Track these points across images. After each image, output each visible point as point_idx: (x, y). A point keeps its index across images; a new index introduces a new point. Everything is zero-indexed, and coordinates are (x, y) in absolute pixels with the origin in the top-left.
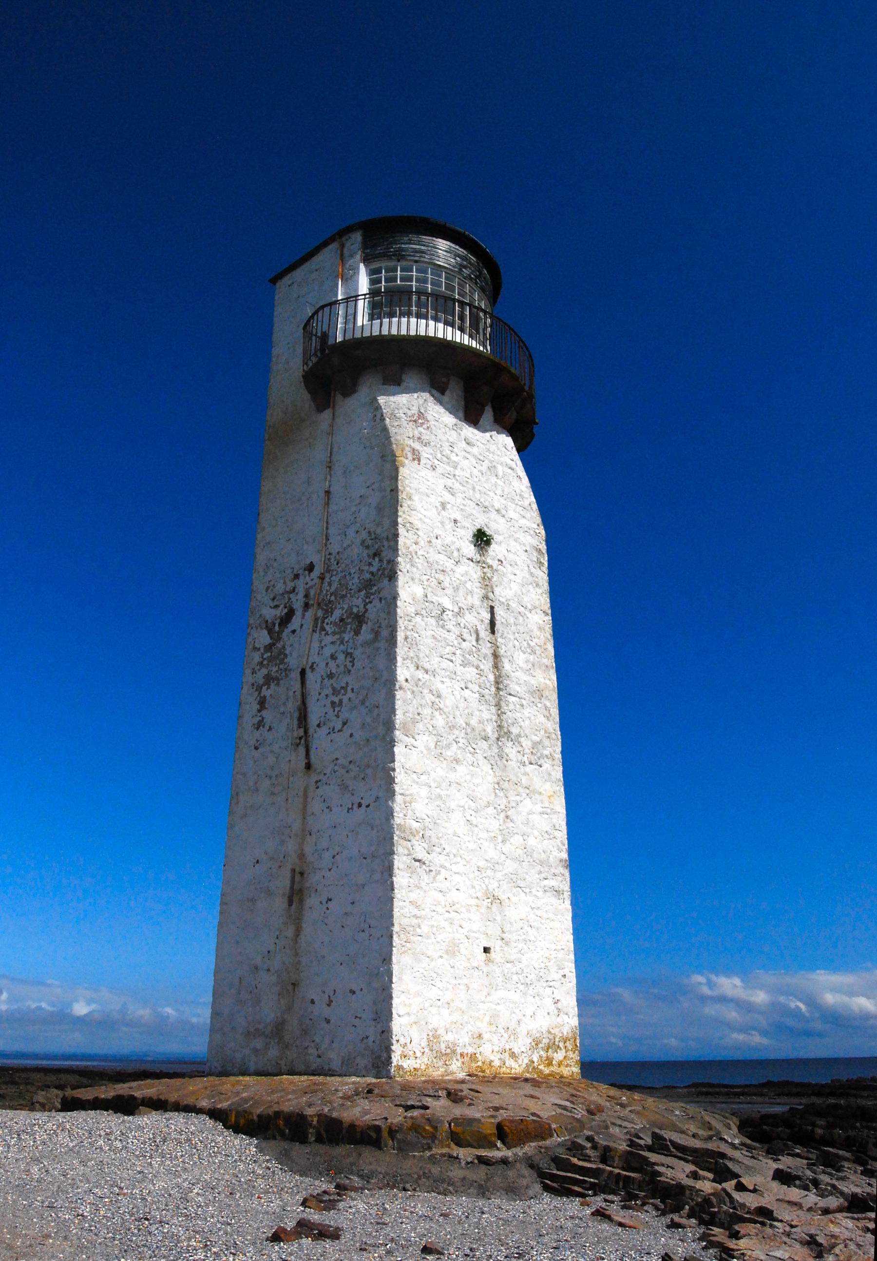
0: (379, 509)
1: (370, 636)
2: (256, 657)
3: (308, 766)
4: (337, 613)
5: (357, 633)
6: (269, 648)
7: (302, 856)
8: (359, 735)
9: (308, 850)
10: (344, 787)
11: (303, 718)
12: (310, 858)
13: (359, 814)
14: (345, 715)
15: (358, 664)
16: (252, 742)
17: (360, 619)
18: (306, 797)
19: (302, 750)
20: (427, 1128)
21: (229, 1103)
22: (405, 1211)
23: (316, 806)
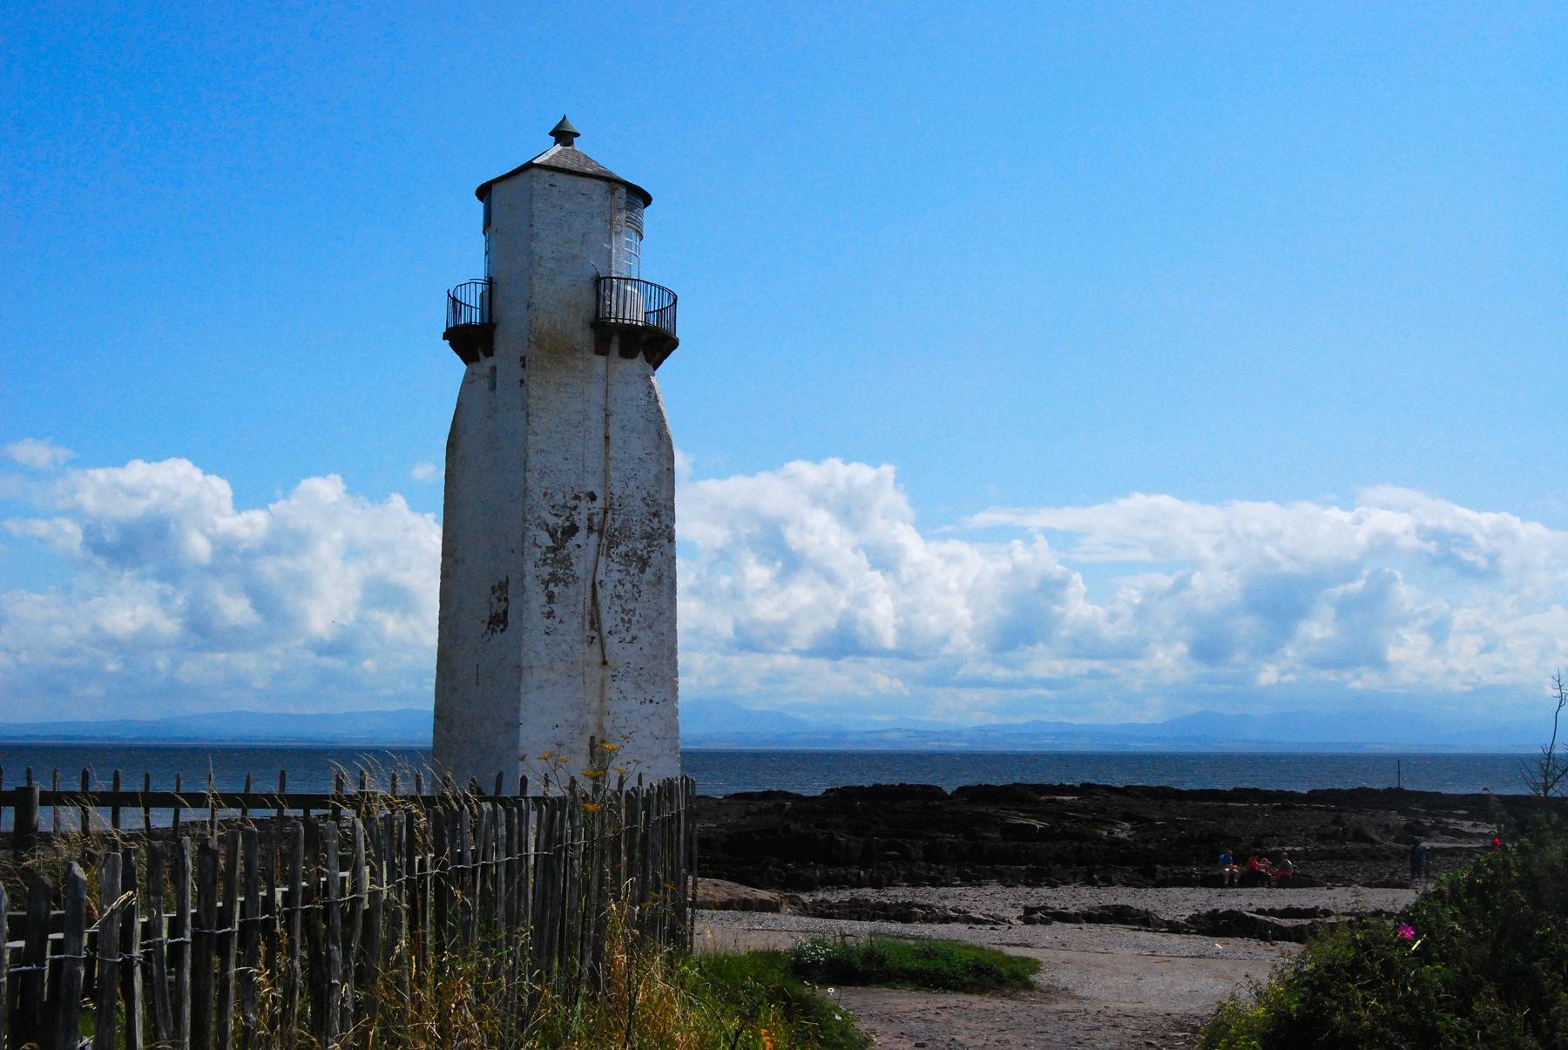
0: (658, 479)
1: (653, 579)
2: (538, 554)
3: (605, 663)
4: (622, 549)
5: (642, 571)
6: (554, 550)
7: (601, 727)
8: (647, 650)
9: (607, 725)
10: (638, 686)
11: (595, 622)
12: (608, 731)
13: (650, 708)
14: (633, 631)
15: (644, 597)
16: (543, 628)
17: (644, 563)
18: (603, 685)
19: (596, 649)
20: (222, 862)
21: (820, 896)
22: (1147, 842)
23: (612, 694)
